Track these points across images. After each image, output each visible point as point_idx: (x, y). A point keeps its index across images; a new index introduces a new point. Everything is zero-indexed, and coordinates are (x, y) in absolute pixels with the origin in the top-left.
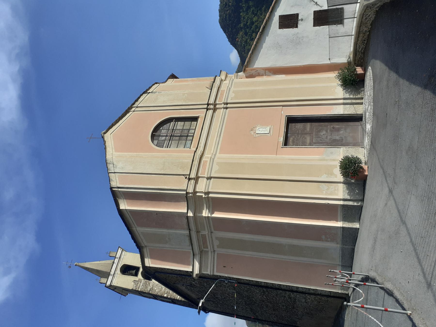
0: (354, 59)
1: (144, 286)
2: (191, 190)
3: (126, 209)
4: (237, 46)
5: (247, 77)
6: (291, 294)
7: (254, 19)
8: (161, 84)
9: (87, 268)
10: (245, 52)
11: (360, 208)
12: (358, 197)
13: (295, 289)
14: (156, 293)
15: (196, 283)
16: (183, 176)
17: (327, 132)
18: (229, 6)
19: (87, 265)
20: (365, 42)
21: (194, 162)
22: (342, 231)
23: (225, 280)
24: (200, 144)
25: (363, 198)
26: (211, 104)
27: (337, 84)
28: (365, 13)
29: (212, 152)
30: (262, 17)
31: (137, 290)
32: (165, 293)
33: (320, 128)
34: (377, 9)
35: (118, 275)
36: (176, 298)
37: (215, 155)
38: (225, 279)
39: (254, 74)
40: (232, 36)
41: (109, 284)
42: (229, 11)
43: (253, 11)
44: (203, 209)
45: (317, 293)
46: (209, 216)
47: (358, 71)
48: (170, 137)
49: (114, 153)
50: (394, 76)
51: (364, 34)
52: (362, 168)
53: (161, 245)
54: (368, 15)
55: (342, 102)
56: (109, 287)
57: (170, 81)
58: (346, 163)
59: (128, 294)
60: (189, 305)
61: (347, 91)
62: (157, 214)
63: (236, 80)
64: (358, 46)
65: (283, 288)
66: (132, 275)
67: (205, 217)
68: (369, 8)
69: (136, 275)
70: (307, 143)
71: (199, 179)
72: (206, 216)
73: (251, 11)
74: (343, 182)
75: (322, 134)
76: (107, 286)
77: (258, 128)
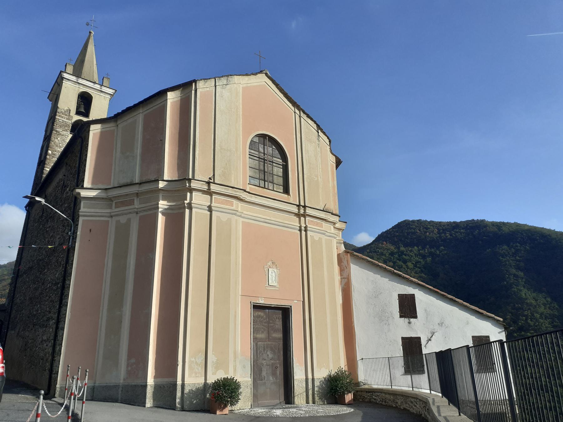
2: (194, 184)
4: (376, 243)
5: (339, 255)
6: (54, 321)
9: (86, 47)
10: (369, 253)
11: (172, 407)
12: (187, 403)
15: (67, 193)
19: (91, 48)
20: (384, 403)
23: (72, 232)
25: (186, 410)
26: (305, 210)
27: (331, 370)
29: (245, 212)
31: (57, 113)
32: (53, 152)
36: (46, 166)
37: (240, 216)
38: (74, 231)
39: (342, 264)
40: (389, 236)
42: (419, 232)
43: (420, 262)
44: (168, 202)
48: (263, 158)
49: (241, 86)
51: (394, 401)
52: (225, 406)
53: (119, 145)
54: (415, 404)
55: (309, 378)
56: (60, 76)
57: (333, 159)
59: (51, 102)
61: (323, 383)
62: (161, 140)
63: (335, 241)
65: (62, 309)
66: (78, 108)
67: (158, 204)
69: (78, 113)
71: (209, 196)
73: (420, 260)
75: (268, 353)
77: (275, 270)
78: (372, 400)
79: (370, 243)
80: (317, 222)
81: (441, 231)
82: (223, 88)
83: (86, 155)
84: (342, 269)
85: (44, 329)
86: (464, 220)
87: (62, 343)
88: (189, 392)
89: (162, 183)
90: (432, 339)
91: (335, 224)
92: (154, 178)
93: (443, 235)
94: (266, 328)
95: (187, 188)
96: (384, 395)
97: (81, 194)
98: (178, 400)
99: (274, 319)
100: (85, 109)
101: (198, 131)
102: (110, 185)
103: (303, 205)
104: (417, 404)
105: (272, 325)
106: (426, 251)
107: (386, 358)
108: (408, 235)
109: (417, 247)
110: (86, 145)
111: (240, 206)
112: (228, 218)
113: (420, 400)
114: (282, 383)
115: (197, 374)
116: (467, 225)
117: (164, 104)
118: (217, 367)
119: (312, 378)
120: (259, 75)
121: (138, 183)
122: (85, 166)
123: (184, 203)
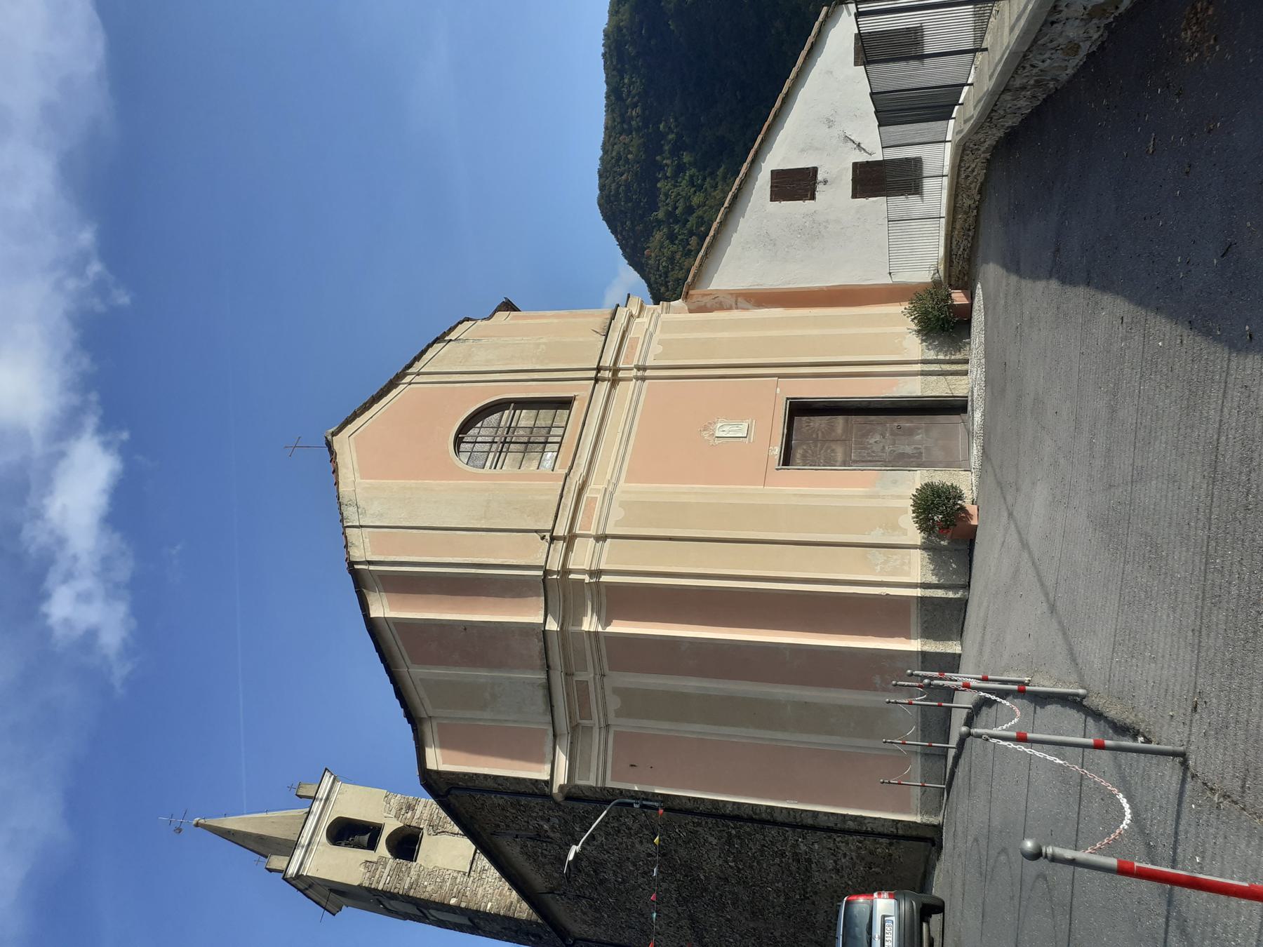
0: (947, 275)
2: (555, 565)
4: (647, 270)
5: (691, 311)
6: (800, 840)
7: (695, 199)
8: (479, 322)
9: (229, 832)
10: (667, 287)
11: (963, 604)
12: (955, 579)
13: (810, 822)
14: (426, 894)
16: (535, 534)
17: (884, 437)
18: (627, 161)
19: (232, 823)
20: (971, 233)
22: (920, 664)
23: (634, 801)
24: (578, 458)
25: (967, 580)
26: (606, 369)
27: (908, 329)
28: (963, 165)
29: (608, 477)
30: (717, 194)
31: (373, 887)
32: (454, 895)
33: (868, 427)
34: (988, 156)
35: (319, 847)
36: (482, 909)
37: (615, 485)
38: (632, 797)
39: (708, 306)
40: (632, 242)
41: (295, 872)
42: (625, 175)
43: (691, 177)
44: (585, 614)
45: (864, 829)
47: (957, 299)
48: (501, 446)
49: (358, 480)
50: (1014, 279)
51: (966, 213)
52: (962, 509)
53: (468, 714)
54: (970, 170)
55: (920, 369)
56: (294, 882)
57: (502, 315)
58: (927, 497)
59: (344, 907)
60: (516, 932)
61: (930, 344)
62: (465, 629)
63: (664, 316)
64: (955, 243)
65: (780, 818)
67: (589, 631)
68: (968, 152)
69: (372, 846)
70: (836, 461)
71: (576, 541)
73: (687, 178)
74: (922, 545)
75: (872, 441)
76: (288, 877)
77: (719, 425)
78: (965, 256)
79: (646, 285)
80: (628, 347)
81: (625, 126)
82: (365, 513)
83: (486, 776)
84: (718, 306)
85: (813, 866)
86: (602, 76)
87: (842, 815)
88: (936, 575)
90: (857, 141)
91: (632, 316)
92: (538, 642)
93: (633, 123)
94: (825, 446)
95: (561, 577)
96: (956, 232)
98: (951, 595)
99: (810, 431)
100: (365, 834)
101: (451, 559)
102: (546, 730)
103: (595, 372)
104: (969, 167)
105: (820, 434)
106: (668, 162)
107: (890, 226)
108: (631, 200)
109: (659, 181)
110: (466, 777)
111: (597, 487)
112: (620, 506)
113: (961, 161)
114: (928, 418)
115: (905, 562)
116: (614, 70)
117: (393, 623)
118: (895, 527)
119: (921, 363)
120: (336, 447)
121: (547, 671)
123: (589, 583)
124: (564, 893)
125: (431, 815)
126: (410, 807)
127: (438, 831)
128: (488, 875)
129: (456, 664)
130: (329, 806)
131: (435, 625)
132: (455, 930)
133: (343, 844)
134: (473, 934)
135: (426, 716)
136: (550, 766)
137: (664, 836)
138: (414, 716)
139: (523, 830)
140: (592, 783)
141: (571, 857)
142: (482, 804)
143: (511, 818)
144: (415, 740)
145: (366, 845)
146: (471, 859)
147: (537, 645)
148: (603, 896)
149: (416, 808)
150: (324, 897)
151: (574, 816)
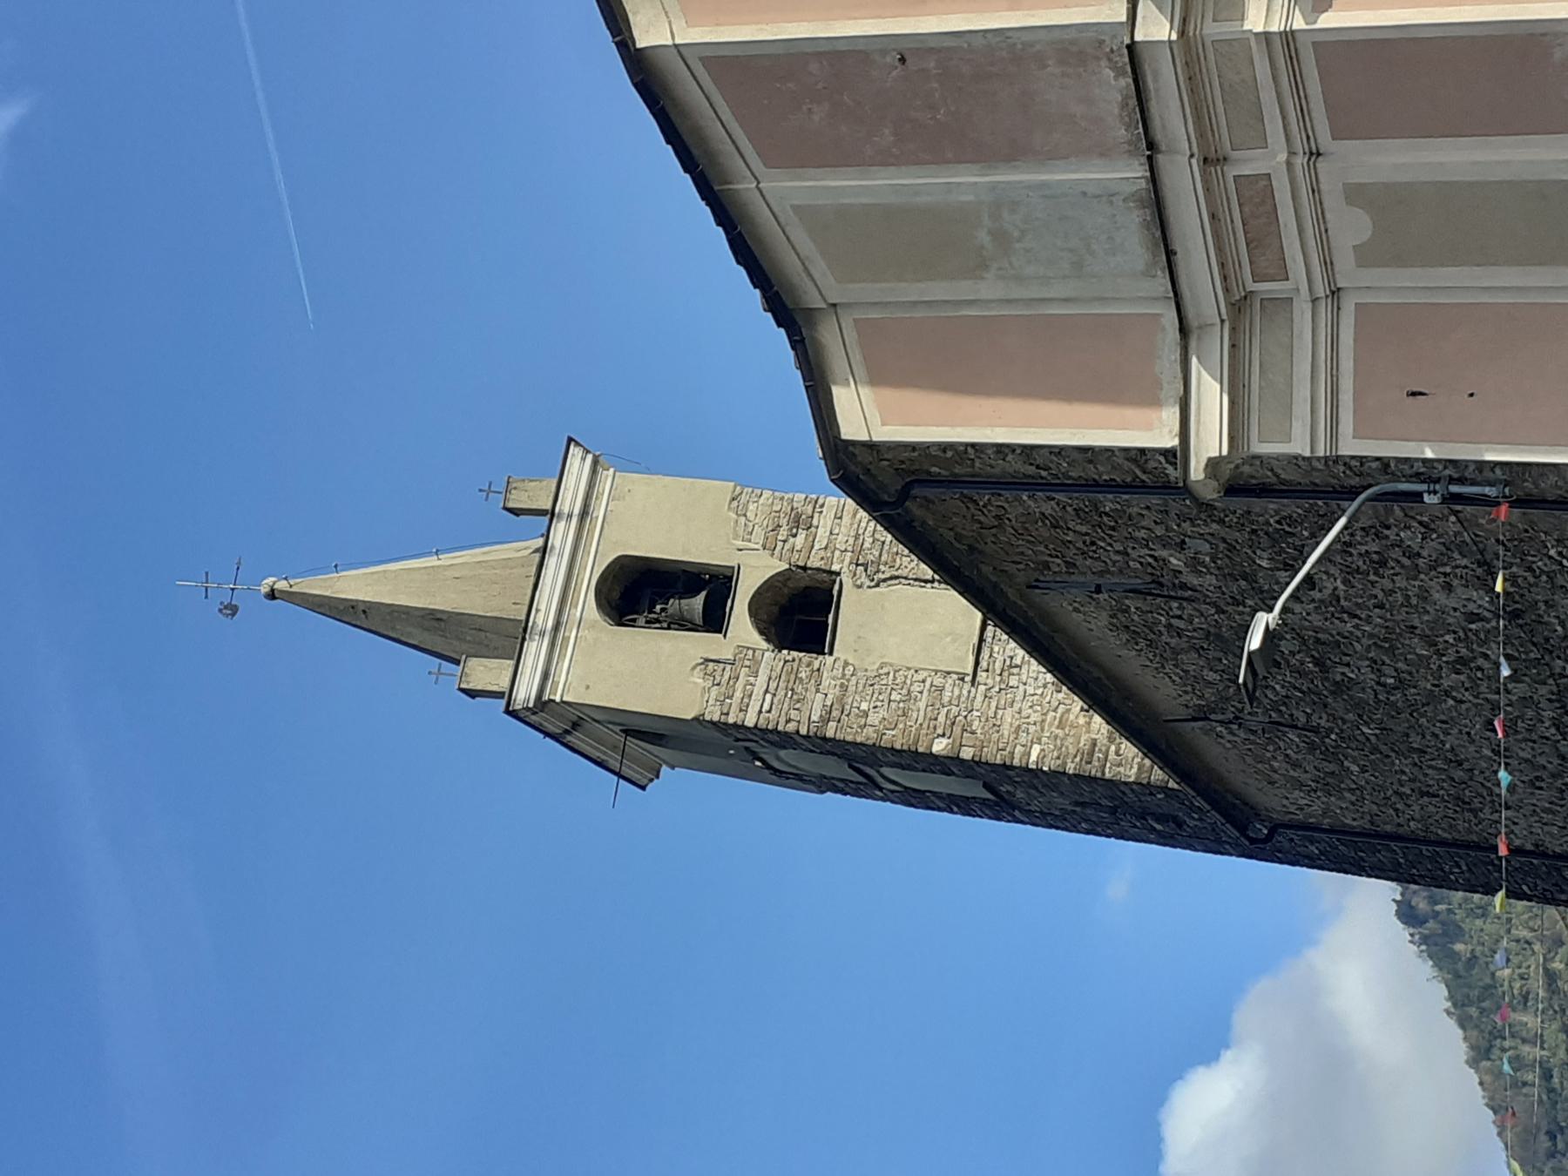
1: (781, 693)
3: (678, 41)
14: (869, 731)
15: (1195, 564)
19: (354, 585)
21: (342, 592)
23: (1424, 487)
31: (731, 720)
32: (940, 731)
36: (1016, 762)
46: (1292, 32)
53: (939, 290)
59: (664, 768)
60: (1113, 811)
62: (903, 60)
66: (682, 623)
69: (714, 620)
72: (1276, 27)
89: (1128, 85)
92: (1116, 78)
97: (1217, 454)
100: (692, 592)
110: (949, 454)
121: (1150, 158)
122: (1059, 451)
124: (1237, 718)
125: (857, 537)
126: (799, 522)
127: (882, 576)
128: (1024, 678)
129: (886, 160)
130: (591, 531)
131: (819, 55)
132: (952, 812)
133: (641, 621)
134: (999, 819)
135: (824, 306)
136: (1177, 410)
137: (1514, 569)
138: (791, 306)
139: (1112, 574)
140: (1299, 446)
141: (1255, 641)
142: (998, 517)
143: (1080, 545)
144: (800, 368)
145: (699, 620)
146: (975, 640)
147: (1113, 86)
148: (1344, 722)
149: (815, 522)
150: (614, 748)
151: (1254, 532)
